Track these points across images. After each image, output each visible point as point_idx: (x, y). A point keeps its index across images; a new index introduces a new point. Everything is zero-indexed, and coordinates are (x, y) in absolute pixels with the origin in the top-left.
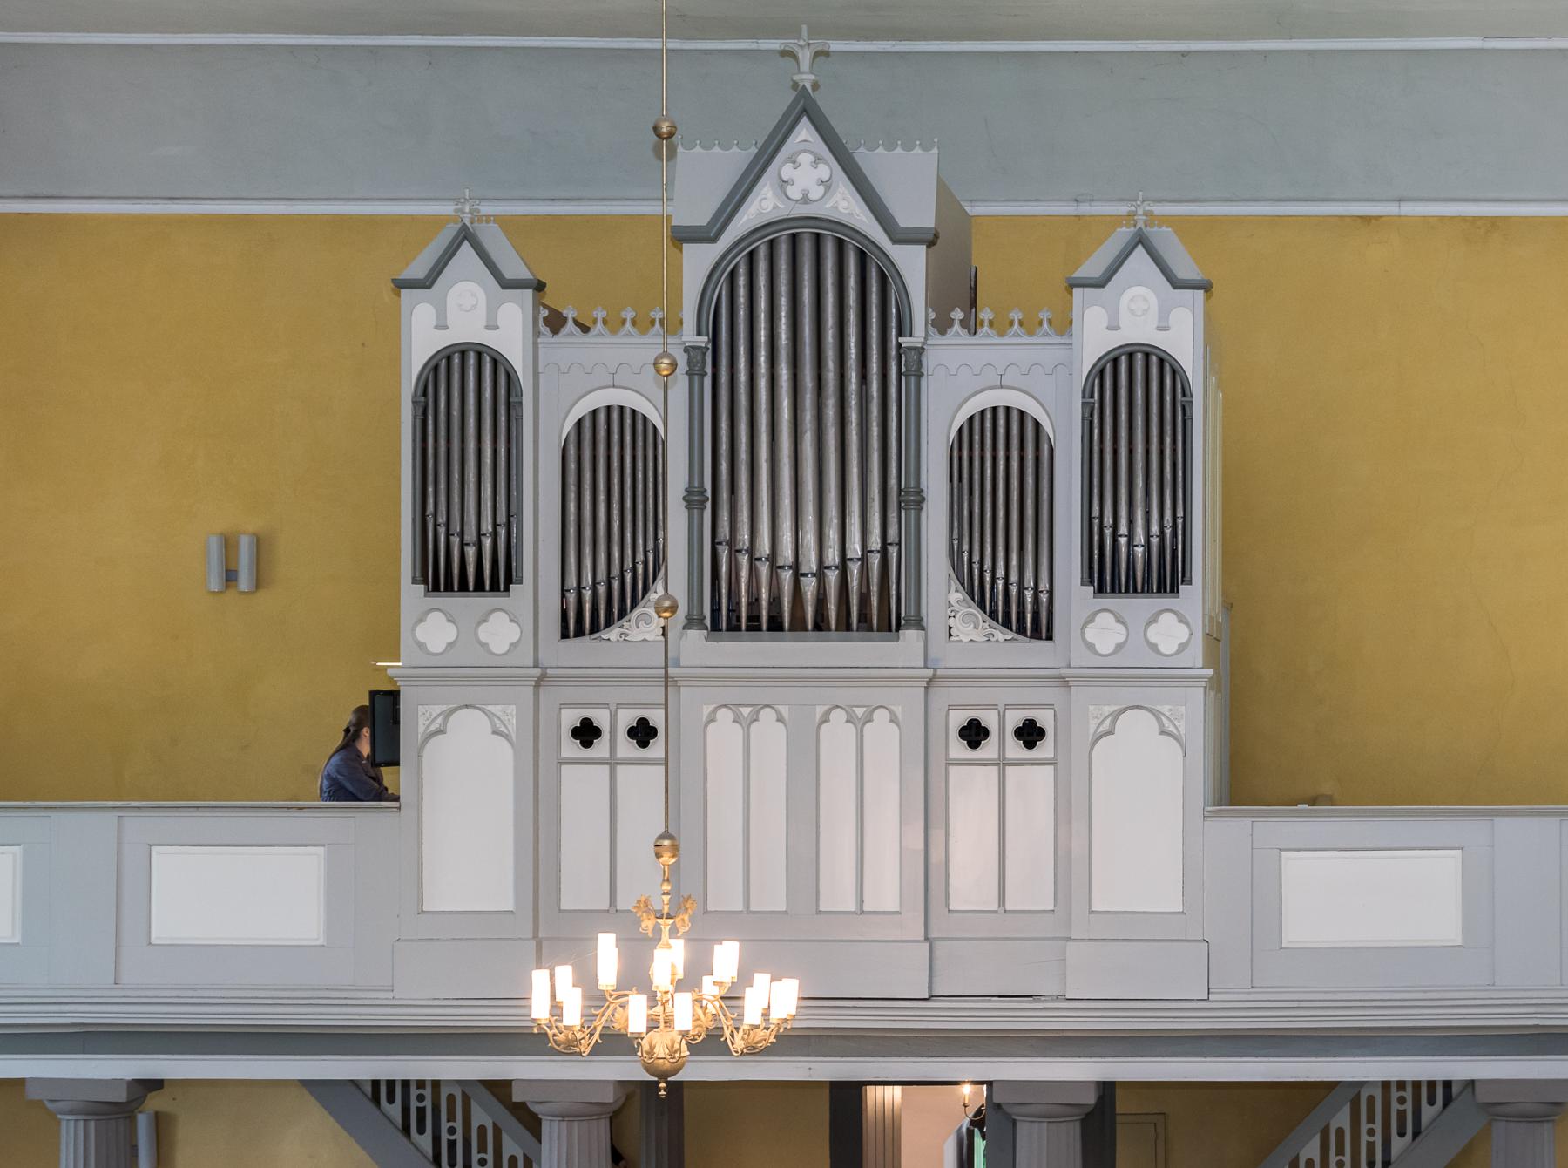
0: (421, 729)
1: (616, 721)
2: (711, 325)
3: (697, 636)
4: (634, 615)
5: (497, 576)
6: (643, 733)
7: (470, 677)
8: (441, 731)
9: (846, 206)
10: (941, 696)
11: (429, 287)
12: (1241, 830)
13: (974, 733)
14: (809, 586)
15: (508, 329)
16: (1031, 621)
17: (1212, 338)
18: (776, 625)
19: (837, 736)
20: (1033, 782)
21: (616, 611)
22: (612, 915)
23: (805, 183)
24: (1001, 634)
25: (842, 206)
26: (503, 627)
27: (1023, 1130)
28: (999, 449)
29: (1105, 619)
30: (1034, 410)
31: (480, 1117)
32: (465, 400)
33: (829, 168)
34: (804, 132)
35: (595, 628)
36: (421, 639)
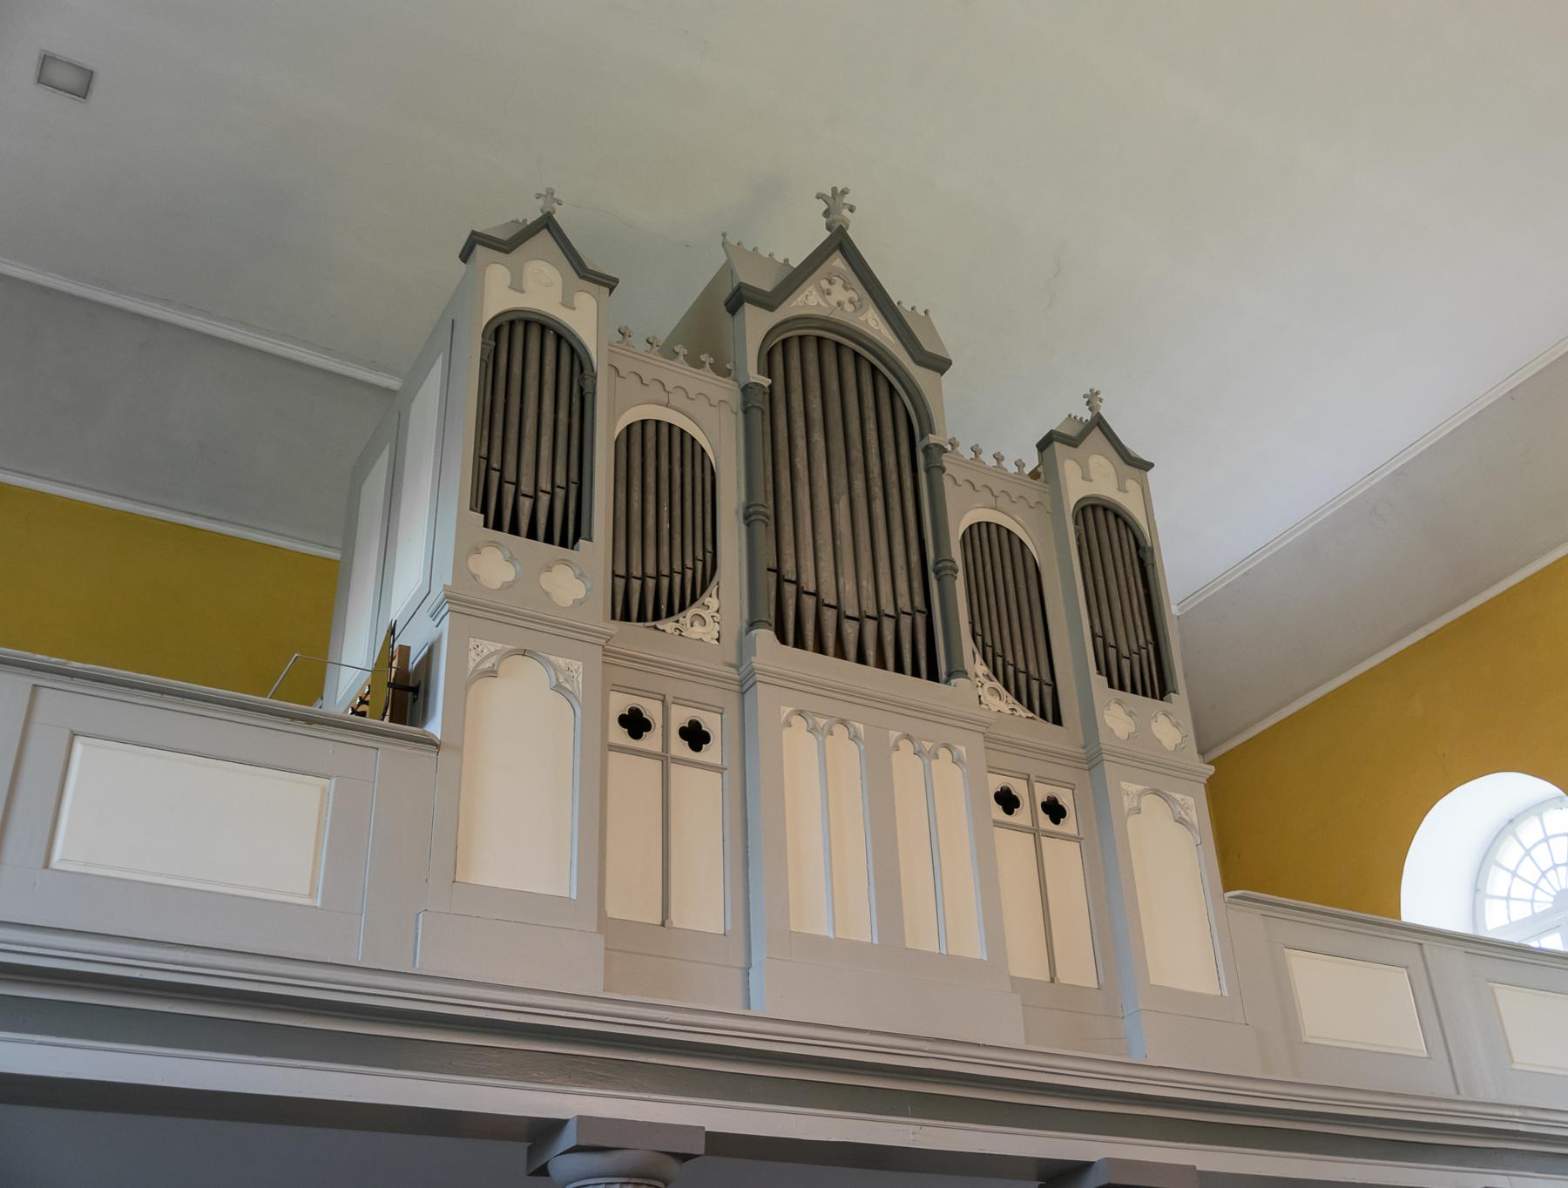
0: (471, 665)
4: (691, 612)
8: (492, 673)
11: (507, 252)
21: (664, 607)
24: (1022, 712)
25: (872, 323)
35: (657, 617)
36: (474, 571)
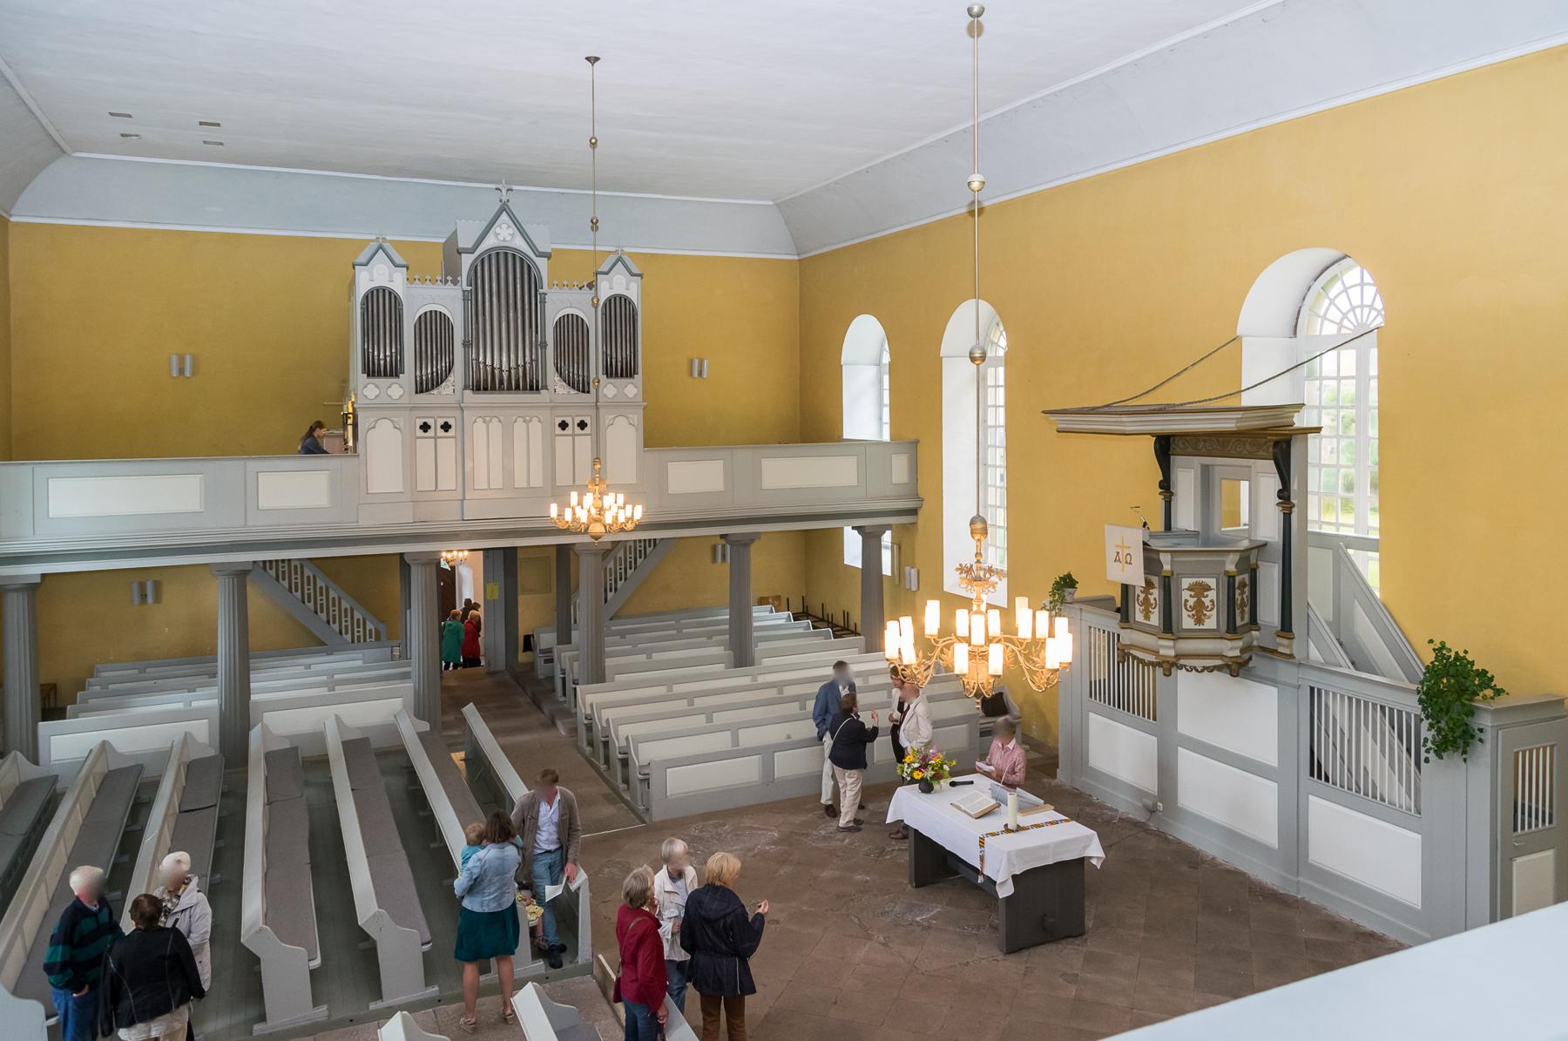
1: (436, 423)
2: (473, 280)
3: (468, 393)
5: (394, 371)
6: (446, 427)
7: (384, 408)
9: (519, 243)
10: (458, 413)
12: (654, 456)
13: (563, 425)
14: (505, 375)
15: (397, 282)
16: (584, 388)
17: (644, 292)
18: (486, 389)
19: (520, 427)
20: (447, 445)
22: (574, 487)
23: (504, 235)
24: (573, 392)
26: (398, 389)
27: (414, 569)
28: (571, 328)
29: (371, 386)
30: (581, 315)
31: (307, 573)
32: (382, 305)
33: (513, 229)
34: (504, 216)
